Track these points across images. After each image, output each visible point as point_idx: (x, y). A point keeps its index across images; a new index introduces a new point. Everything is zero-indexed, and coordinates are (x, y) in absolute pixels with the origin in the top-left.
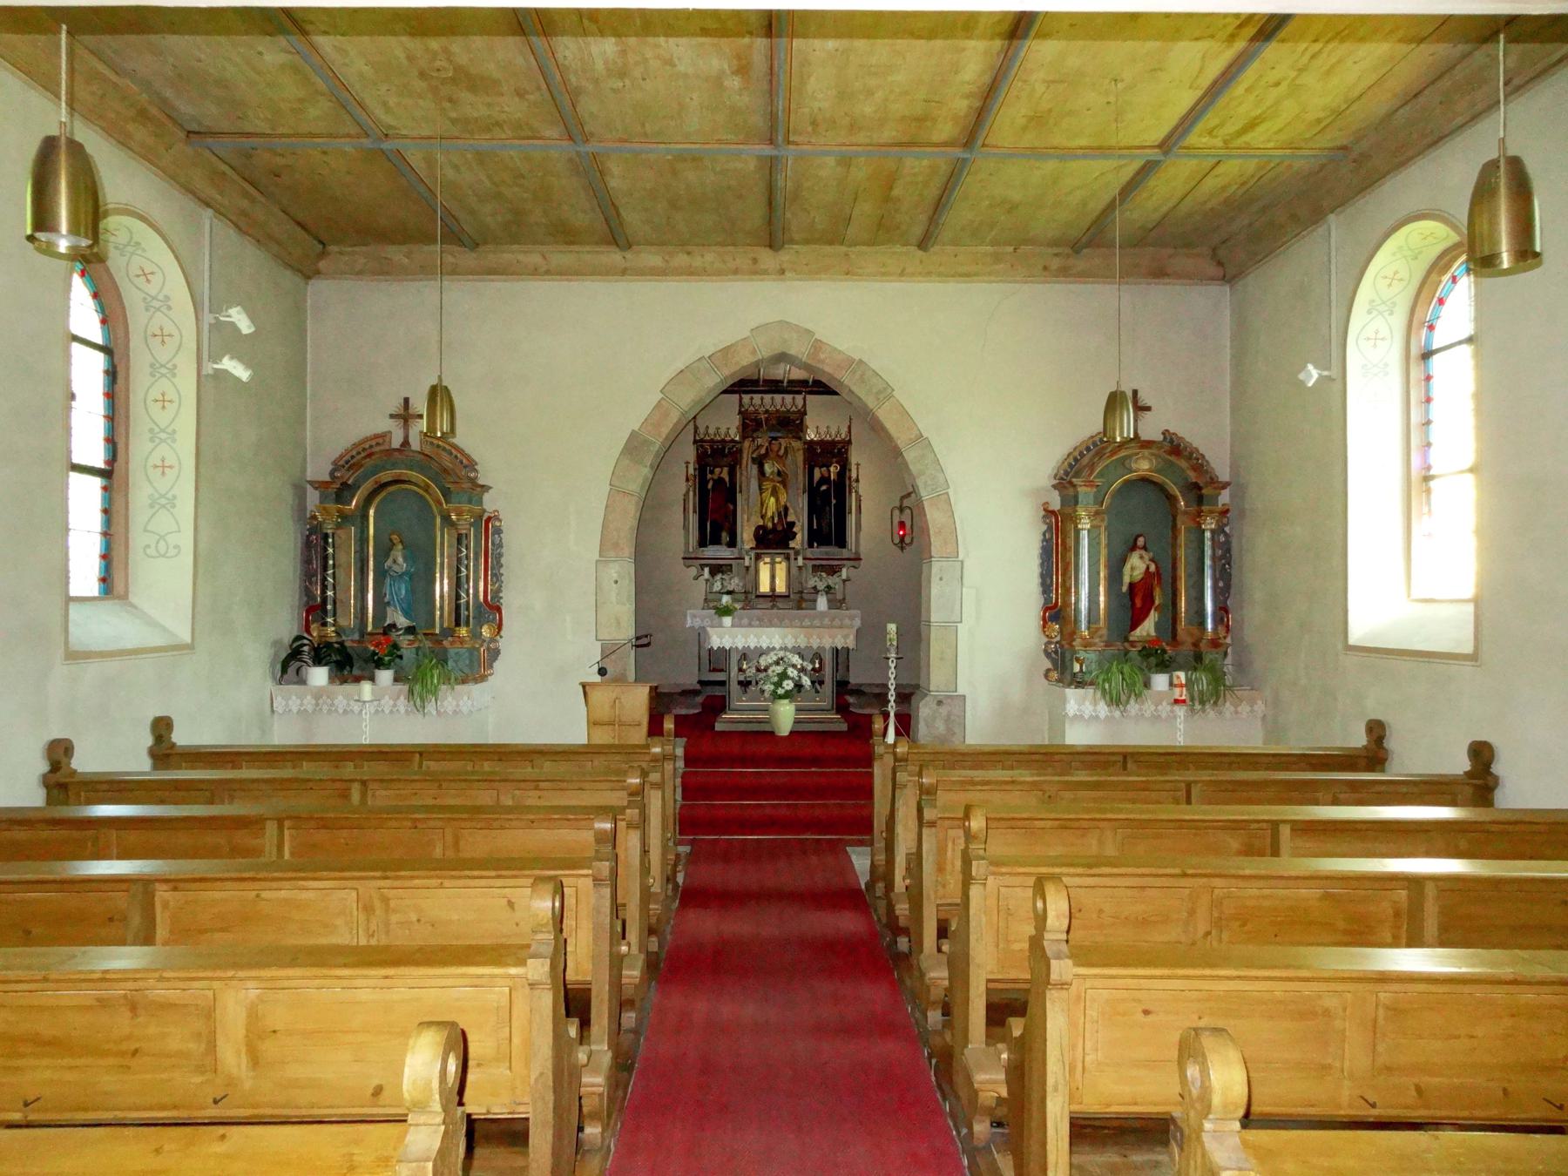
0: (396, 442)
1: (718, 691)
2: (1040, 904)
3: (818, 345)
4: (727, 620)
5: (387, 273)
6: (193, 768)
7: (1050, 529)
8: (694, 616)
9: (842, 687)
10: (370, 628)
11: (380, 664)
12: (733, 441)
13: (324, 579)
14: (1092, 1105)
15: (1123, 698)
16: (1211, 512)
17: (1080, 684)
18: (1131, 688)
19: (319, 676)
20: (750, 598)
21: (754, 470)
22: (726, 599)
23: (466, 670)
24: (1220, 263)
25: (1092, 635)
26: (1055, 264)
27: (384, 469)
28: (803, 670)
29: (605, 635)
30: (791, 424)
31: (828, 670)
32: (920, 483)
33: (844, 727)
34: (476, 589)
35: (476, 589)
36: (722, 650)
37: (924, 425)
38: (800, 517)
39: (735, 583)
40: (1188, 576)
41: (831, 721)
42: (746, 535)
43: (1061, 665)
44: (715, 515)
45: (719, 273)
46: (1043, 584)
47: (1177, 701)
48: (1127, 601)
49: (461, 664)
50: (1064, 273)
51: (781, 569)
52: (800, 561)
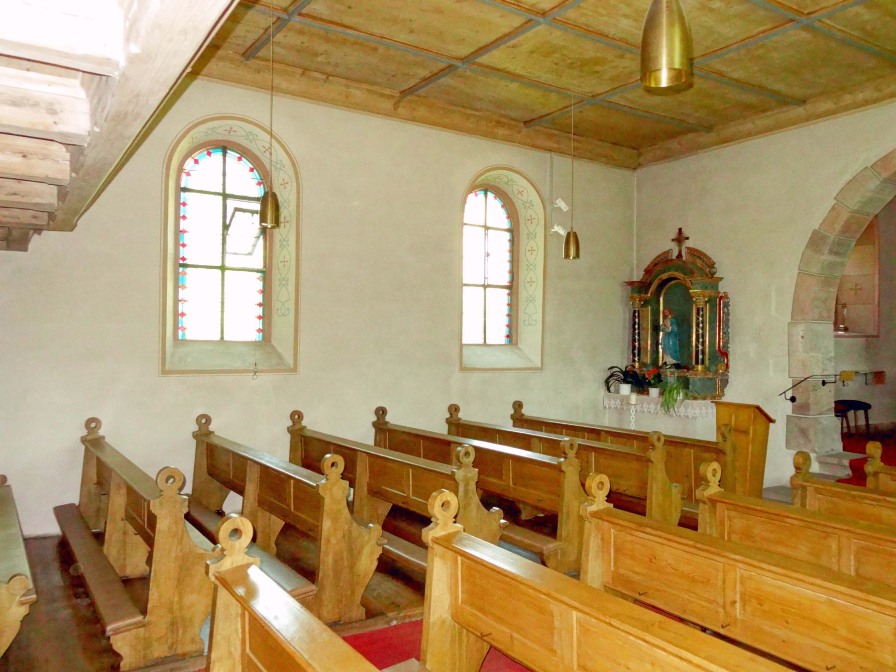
0: (675, 254)
6: (522, 427)
19: (625, 389)
27: (664, 272)
29: (795, 374)
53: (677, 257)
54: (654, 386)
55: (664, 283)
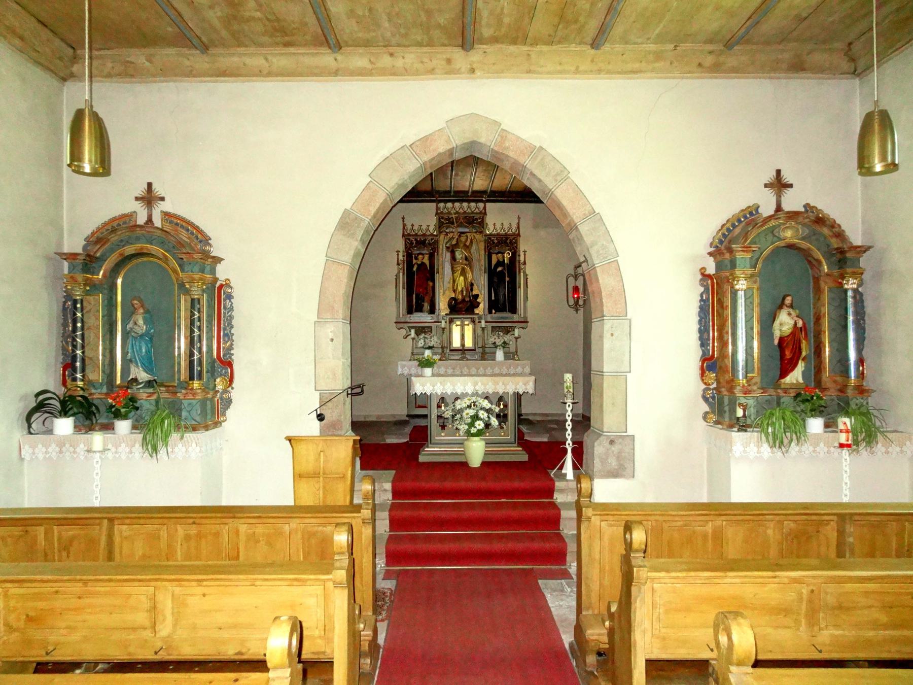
0: (141, 219)
1: (422, 422)
2: (628, 536)
3: (504, 134)
4: (428, 371)
5: (132, 76)
7: (706, 289)
8: (403, 367)
9: (521, 420)
10: (118, 382)
11: (118, 415)
12: (432, 235)
13: (74, 340)
14: (658, 654)
15: (786, 441)
16: (854, 273)
17: (743, 428)
18: (787, 428)
19: (64, 426)
20: (446, 351)
21: (448, 255)
22: (428, 353)
23: (198, 418)
24: (853, 60)
25: (749, 380)
26: (709, 60)
27: (128, 243)
28: (488, 411)
29: (323, 386)
30: (476, 222)
31: (511, 412)
32: (593, 251)
33: (525, 457)
34: (208, 347)
35: (208, 347)
36: (424, 395)
37: (598, 202)
38: (482, 290)
39: (434, 341)
40: (831, 330)
41: (513, 453)
42: (443, 306)
43: (722, 408)
44: (418, 287)
45: (417, 73)
46: (701, 338)
47: (842, 446)
48: (777, 354)
49: (193, 413)
50: (716, 69)
51: (469, 330)
52: (483, 324)
53: (147, 223)
54: (125, 417)
55: (125, 260)
